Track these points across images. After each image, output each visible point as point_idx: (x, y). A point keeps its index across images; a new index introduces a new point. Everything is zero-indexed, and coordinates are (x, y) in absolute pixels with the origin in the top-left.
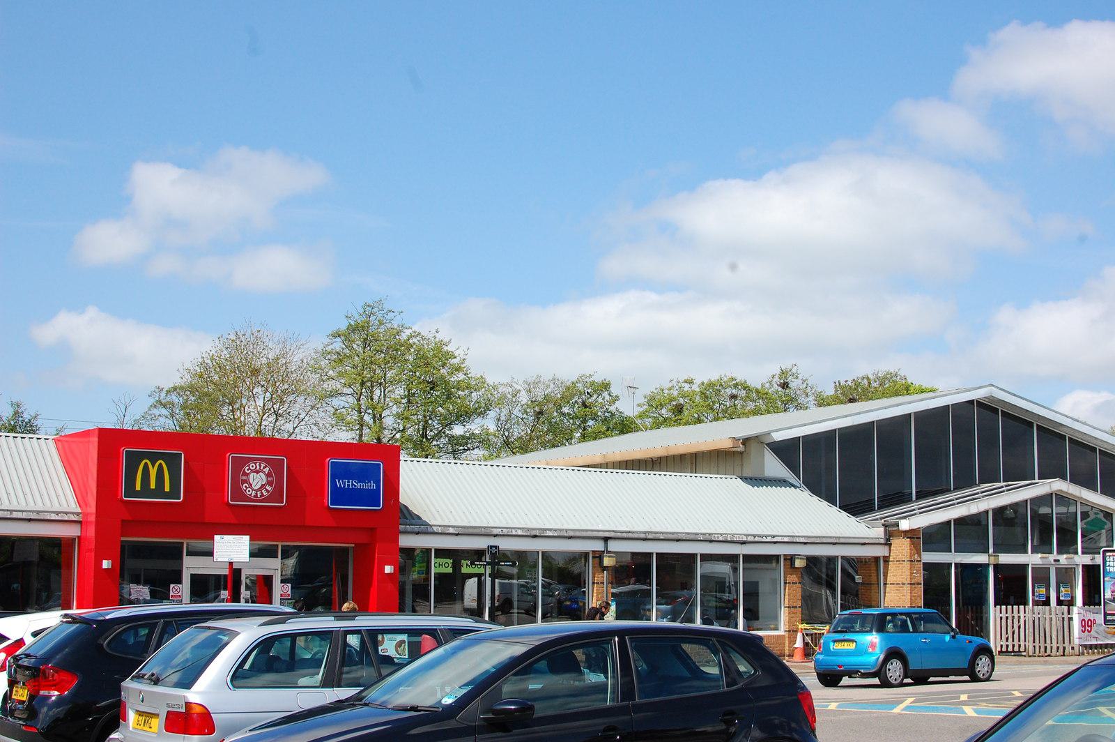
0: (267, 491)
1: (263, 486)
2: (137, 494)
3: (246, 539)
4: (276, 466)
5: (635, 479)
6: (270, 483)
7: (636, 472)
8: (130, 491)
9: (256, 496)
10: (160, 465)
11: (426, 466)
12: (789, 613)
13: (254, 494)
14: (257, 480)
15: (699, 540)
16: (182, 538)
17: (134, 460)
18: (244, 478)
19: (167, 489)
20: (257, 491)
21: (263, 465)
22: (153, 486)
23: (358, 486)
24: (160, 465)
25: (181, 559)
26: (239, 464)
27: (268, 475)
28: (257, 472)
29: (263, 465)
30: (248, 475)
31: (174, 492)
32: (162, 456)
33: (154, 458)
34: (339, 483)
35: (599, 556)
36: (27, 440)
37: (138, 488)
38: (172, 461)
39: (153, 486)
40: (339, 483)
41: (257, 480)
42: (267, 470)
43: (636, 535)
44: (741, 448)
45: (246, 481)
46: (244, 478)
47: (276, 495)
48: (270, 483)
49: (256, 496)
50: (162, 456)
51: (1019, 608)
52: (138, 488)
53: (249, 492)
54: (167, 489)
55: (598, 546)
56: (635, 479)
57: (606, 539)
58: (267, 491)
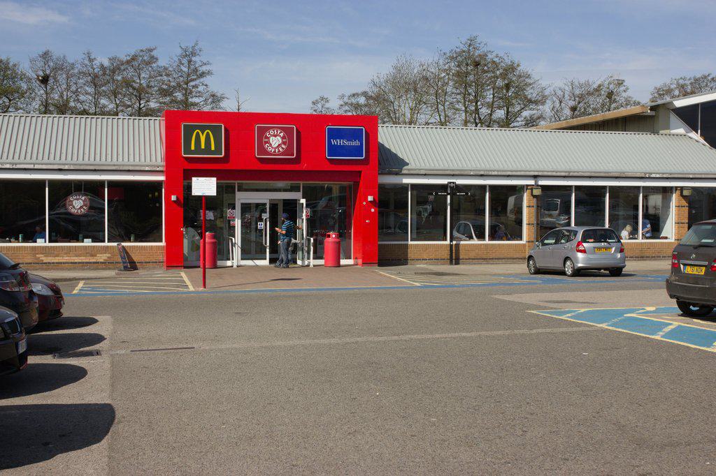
0: (283, 148)
1: (279, 145)
2: (193, 152)
3: (214, 179)
4: (288, 132)
5: (588, 137)
6: (85, 205)
7: (597, 132)
8: (188, 150)
9: (275, 152)
10: (208, 133)
11: (544, 135)
12: (678, 228)
13: (273, 150)
14: (275, 142)
15: (470, 175)
16: (234, 180)
17: (189, 131)
18: (266, 140)
19: (213, 148)
20: (275, 148)
21: (279, 132)
22: (203, 147)
23: (347, 143)
24: (208, 133)
25: (235, 193)
26: (262, 132)
27: (283, 138)
28: (275, 136)
29: (279, 132)
30: (268, 138)
31: (218, 150)
32: (208, 127)
33: (203, 129)
34: (334, 142)
35: (531, 188)
36: (430, 129)
37: (193, 148)
38: (216, 131)
39: (203, 147)
40: (334, 142)
41: (275, 142)
42: (282, 135)
43: (558, 174)
44: (653, 113)
45: (72, 205)
46: (266, 140)
47: (288, 151)
48: (85, 205)
49: (275, 152)
50: (208, 127)
51: (463, 259)
52: (193, 148)
53: (269, 149)
54: (213, 148)
55: (532, 182)
56: (588, 137)
57: (535, 177)
58: (283, 148)
